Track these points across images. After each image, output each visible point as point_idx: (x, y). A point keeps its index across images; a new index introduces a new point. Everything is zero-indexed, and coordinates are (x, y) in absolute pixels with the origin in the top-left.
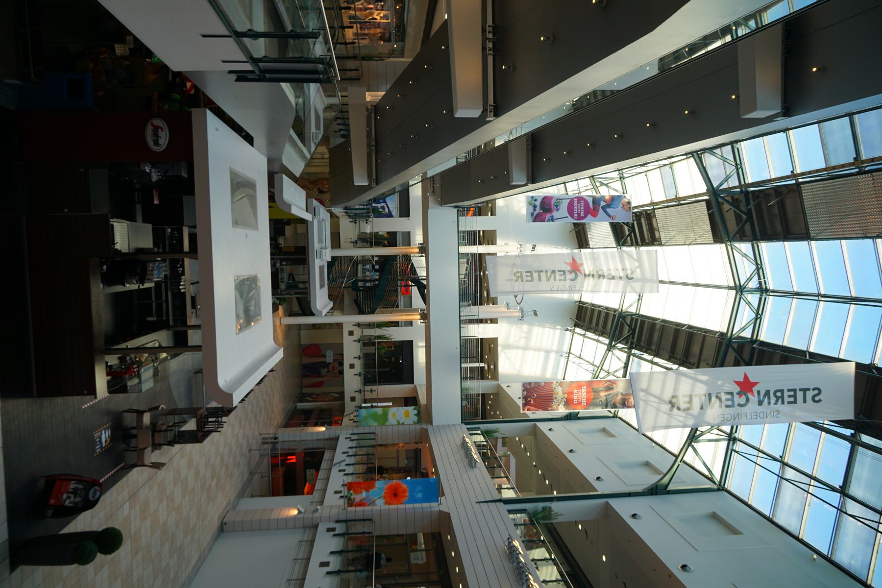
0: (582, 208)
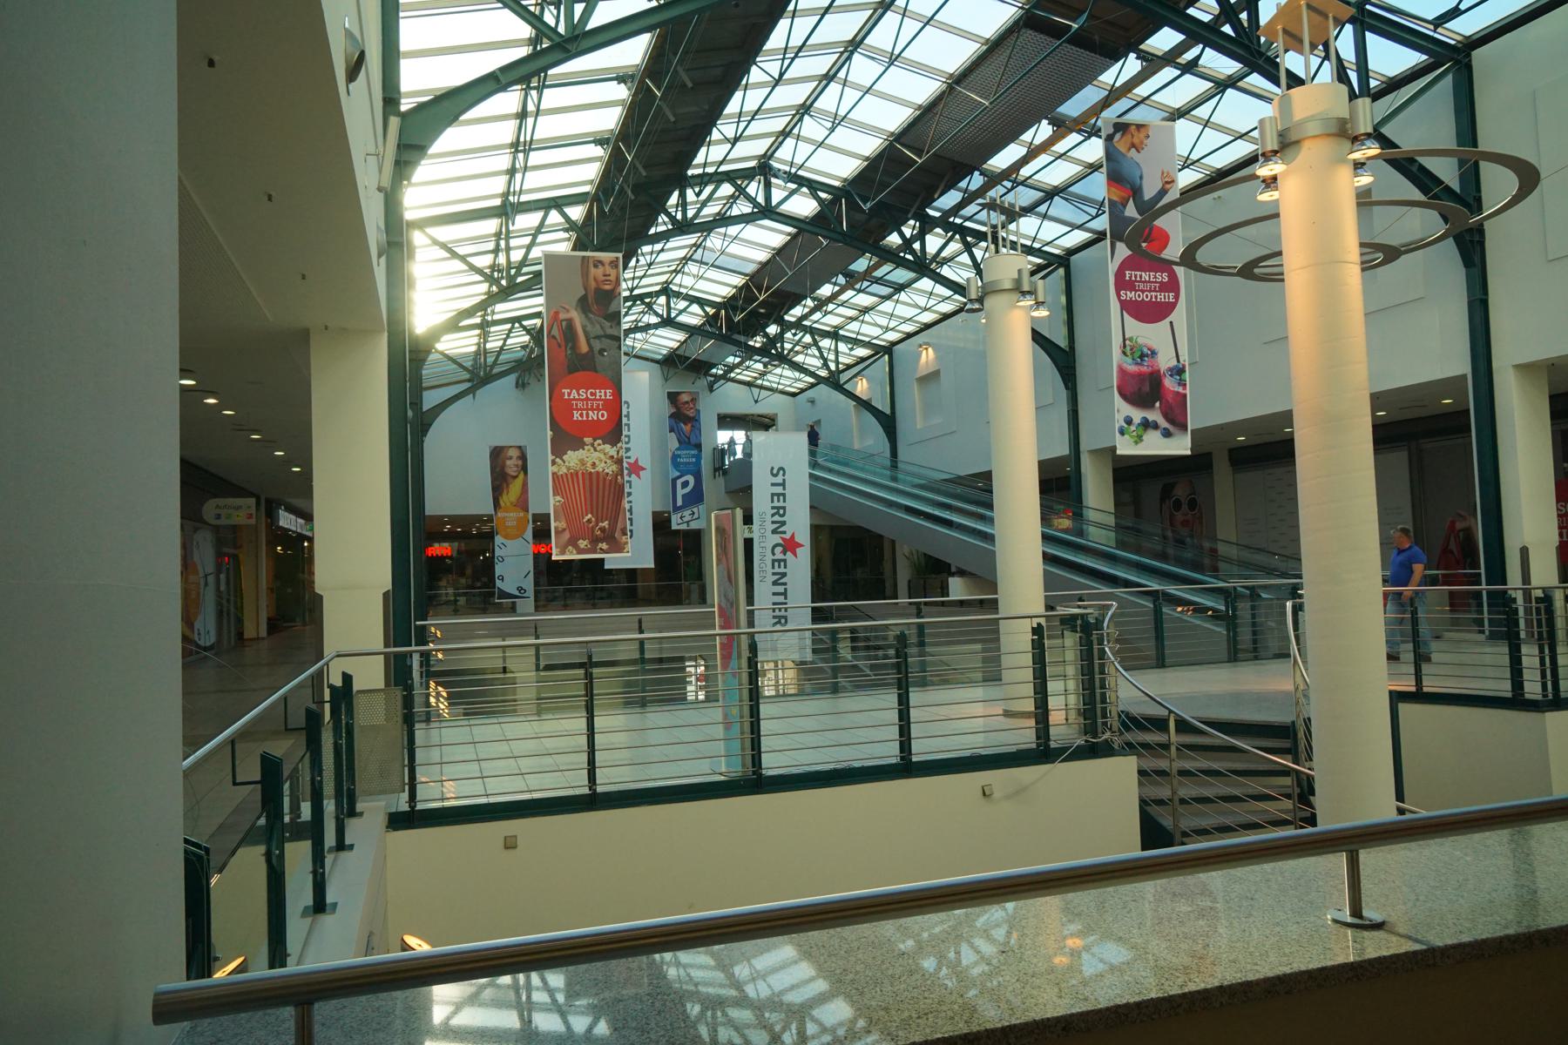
0: (1145, 276)
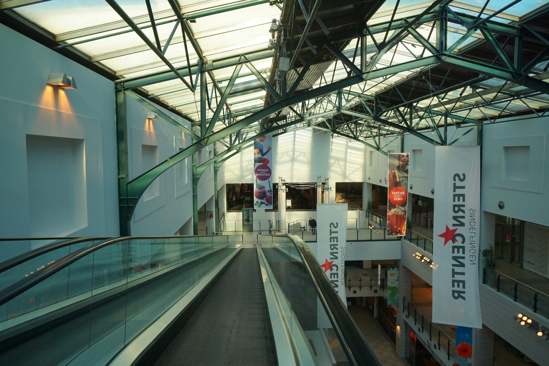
0: (263, 170)
